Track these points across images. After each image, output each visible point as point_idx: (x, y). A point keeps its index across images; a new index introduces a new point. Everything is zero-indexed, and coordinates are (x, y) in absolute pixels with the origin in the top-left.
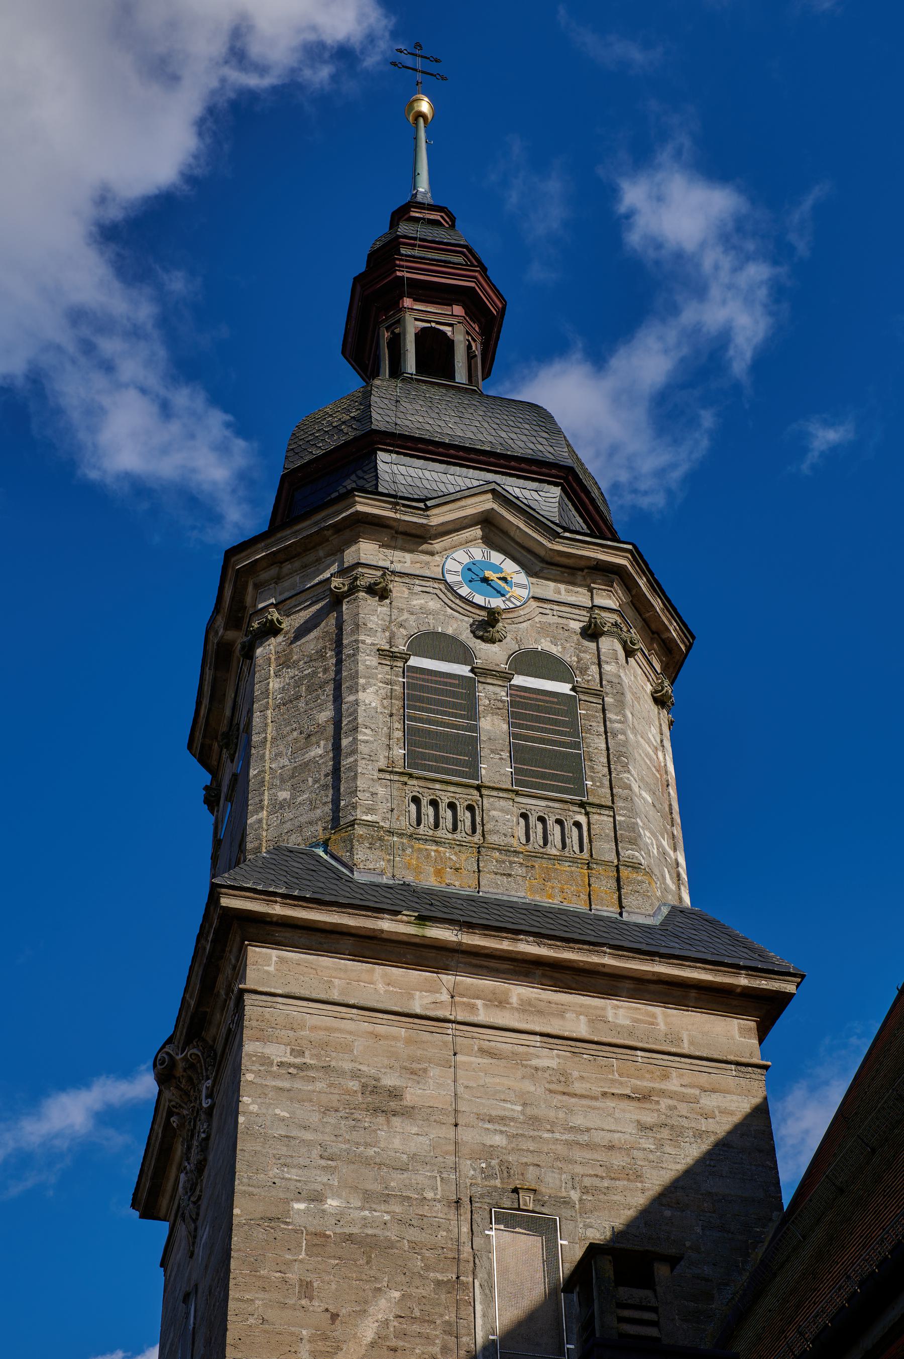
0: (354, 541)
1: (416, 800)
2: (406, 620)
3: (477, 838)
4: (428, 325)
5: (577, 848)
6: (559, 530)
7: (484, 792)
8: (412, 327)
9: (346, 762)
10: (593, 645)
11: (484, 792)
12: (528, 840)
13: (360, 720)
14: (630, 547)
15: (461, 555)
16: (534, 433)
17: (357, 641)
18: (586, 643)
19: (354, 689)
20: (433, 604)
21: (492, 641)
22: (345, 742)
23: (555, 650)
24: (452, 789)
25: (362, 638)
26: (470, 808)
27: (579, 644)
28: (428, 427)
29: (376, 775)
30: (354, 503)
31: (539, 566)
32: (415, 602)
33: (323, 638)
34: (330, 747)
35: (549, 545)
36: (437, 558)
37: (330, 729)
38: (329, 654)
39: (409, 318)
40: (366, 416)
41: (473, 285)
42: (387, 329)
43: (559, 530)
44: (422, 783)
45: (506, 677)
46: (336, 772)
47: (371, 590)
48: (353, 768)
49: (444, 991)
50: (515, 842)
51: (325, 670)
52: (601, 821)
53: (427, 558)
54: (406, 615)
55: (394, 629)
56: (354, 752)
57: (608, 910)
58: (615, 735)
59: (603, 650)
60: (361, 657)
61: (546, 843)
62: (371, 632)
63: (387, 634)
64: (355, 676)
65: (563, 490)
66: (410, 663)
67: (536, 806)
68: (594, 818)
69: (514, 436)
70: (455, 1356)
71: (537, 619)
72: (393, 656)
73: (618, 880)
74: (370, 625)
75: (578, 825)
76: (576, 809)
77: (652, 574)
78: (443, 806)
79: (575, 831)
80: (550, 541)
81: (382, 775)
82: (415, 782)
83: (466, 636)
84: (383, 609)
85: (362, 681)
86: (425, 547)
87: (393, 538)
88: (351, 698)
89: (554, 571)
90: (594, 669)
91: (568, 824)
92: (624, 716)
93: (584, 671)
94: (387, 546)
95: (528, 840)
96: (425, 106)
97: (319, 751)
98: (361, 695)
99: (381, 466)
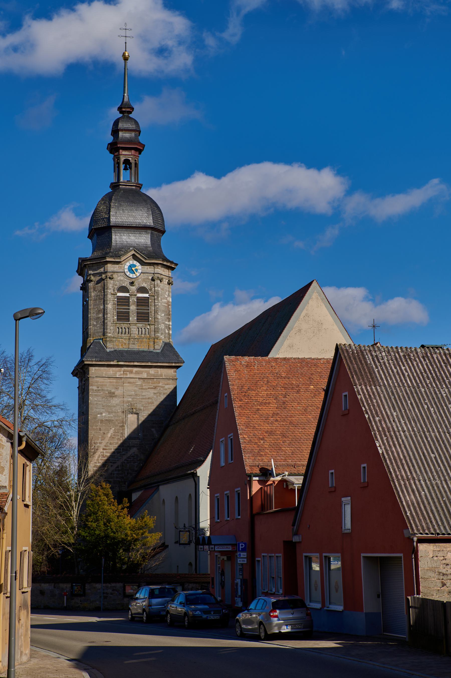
0: (107, 264)
1: (118, 328)
4: (126, 158)
6: (147, 258)
9: (106, 321)
10: (153, 282)
11: (131, 325)
15: (128, 264)
20: (122, 278)
22: (105, 316)
24: (125, 324)
25: (108, 291)
26: (128, 328)
27: (151, 282)
30: (106, 259)
31: (143, 264)
36: (123, 265)
37: (103, 310)
38: (102, 292)
39: (121, 156)
40: (109, 219)
42: (117, 158)
46: (104, 322)
47: (110, 278)
48: (107, 323)
50: (136, 335)
51: (102, 296)
52: (153, 327)
53: (121, 265)
54: (117, 282)
55: (114, 286)
56: (107, 319)
57: (151, 349)
58: (156, 306)
62: (110, 289)
64: (107, 301)
66: (117, 295)
72: (114, 294)
73: (154, 342)
74: (110, 287)
75: (148, 328)
76: (148, 325)
79: (147, 329)
82: (118, 324)
84: (112, 282)
85: (108, 302)
88: (106, 321)
89: (146, 264)
90: (153, 288)
93: (151, 290)
97: (101, 315)
99: (113, 237)
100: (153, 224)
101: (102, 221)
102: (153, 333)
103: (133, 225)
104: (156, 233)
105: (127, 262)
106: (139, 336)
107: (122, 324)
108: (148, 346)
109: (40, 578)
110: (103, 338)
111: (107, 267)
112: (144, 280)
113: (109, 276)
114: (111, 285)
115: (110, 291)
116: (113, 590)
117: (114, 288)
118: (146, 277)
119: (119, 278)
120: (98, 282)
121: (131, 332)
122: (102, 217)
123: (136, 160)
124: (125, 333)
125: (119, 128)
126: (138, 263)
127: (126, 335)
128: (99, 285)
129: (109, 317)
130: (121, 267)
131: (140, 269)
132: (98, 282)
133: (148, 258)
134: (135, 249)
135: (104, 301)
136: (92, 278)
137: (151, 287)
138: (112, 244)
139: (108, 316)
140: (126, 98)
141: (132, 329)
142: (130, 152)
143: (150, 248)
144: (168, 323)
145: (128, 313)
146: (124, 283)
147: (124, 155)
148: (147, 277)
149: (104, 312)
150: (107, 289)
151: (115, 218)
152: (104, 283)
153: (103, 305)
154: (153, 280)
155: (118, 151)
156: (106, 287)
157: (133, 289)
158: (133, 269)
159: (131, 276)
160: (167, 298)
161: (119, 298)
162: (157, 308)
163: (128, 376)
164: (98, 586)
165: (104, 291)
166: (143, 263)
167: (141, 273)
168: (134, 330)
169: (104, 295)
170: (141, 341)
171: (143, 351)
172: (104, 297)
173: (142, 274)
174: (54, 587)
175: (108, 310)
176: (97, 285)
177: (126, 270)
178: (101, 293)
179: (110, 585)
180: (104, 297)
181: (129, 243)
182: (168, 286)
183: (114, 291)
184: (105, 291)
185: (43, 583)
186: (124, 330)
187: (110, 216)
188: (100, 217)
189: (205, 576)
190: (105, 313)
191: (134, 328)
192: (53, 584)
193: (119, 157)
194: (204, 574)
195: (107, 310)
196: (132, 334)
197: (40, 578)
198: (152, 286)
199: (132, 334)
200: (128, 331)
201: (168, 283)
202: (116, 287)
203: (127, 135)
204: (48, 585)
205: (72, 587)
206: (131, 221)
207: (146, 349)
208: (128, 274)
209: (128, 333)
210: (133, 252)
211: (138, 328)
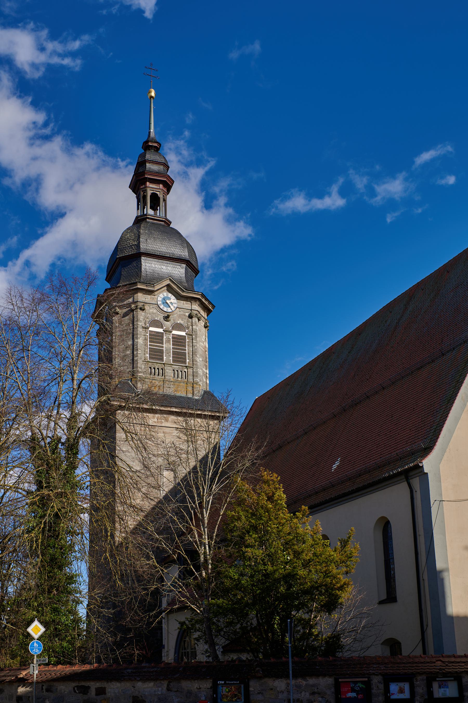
0: (137, 293)
1: (150, 368)
2: (148, 316)
3: (163, 377)
4: (153, 192)
5: (184, 378)
6: (185, 290)
7: (165, 365)
8: (149, 193)
9: (135, 358)
10: (191, 320)
11: (165, 365)
12: (174, 377)
13: (138, 348)
14: (201, 293)
15: (161, 296)
16: (180, 248)
17: (137, 324)
18: (189, 319)
19: (137, 338)
20: (155, 311)
21: (168, 321)
22: (135, 353)
23: (182, 322)
24: (158, 364)
25: (139, 323)
26: (162, 369)
27: (188, 320)
28: (154, 249)
29: (142, 362)
30: (137, 285)
31: (179, 297)
32: (151, 311)
33: (129, 319)
34: (131, 352)
35: (182, 294)
36: (156, 296)
37: (131, 347)
39: (148, 189)
40: (138, 246)
41: (165, 179)
43: (185, 290)
44: (152, 363)
45: (171, 332)
46: (133, 359)
48: (137, 361)
49: (156, 418)
50: (171, 378)
51: (130, 330)
52: (190, 370)
53: (153, 296)
54: (149, 315)
55: (146, 319)
56: (137, 356)
57: (190, 396)
59: (193, 322)
60: (139, 329)
61: (178, 377)
62: (141, 322)
63: (144, 321)
64: (137, 334)
65: (186, 265)
67: (176, 367)
68: (189, 370)
69: (175, 250)
70: (2, 305)
71: (178, 313)
72: (146, 328)
74: (141, 319)
75: (185, 372)
76: (185, 368)
77: (206, 297)
78: (156, 369)
79: (184, 373)
80: (182, 292)
81: (143, 362)
82: (150, 363)
83: (162, 320)
84: (143, 314)
85: (139, 336)
86: (153, 294)
87: (146, 292)
88: (136, 358)
89: (183, 299)
90: (191, 327)
91: (183, 372)
92: (197, 341)
94: (144, 294)
95: (174, 377)
96: (153, 94)
97: (129, 352)
98: (139, 340)
100: (188, 257)
101: (130, 249)
102: (190, 378)
103: (166, 256)
104: (190, 270)
105: (160, 293)
106: (174, 379)
107: (155, 364)
108: (186, 392)
109: (129, 671)
110: (132, 379)
111: (138, 296)
112: (180, 316)
113: (140, 306)
114: (142, 317)
115: (141, 324)
116: (313, 693)
117: (146, 321)
118: (182, 313)
119: (151, 311)
120: (125, 315)
121: (166, 374)
122: (129, 244)
123: (164, 196)
124: (159, 375)
125: (146, 159)
126: (172, 296)
127: (159, 377)
128: (127, 317)
129: (140, 354)
130: (154, 298)
131: (175, 303)
132: (125, 315)
133: (186, 290)
134: (171, 278)
135: (133, 336)
136: (118, 310)
137: (188, 325)
138: (142, 274)
139: (139, 352)
140: (152, 134)
141: (167, 371)
142: (158, 186)
143: (185, 283)
144: (205, 371)
145: (162, 352)
146: (157, 317)
147: (151, 188)
148: (184, 313)
149: (134, 348)
150: (137, 321)
151: (145, 245)
152: (133, 315)
153: (131, 340)
154: (191, 317)
155: (145, 184)
156: (135, 319)
157: (168, 325)
158: (168, 302)
159: (165, 309)
160: (204, 342)
161: (152, 334)
162: (196, 349)
163: (163, 425)
164: (280, 684)
165: (133, 324)
166: (179, 297)
167: (177, 307)
168: (169, 372)
169: (133, 328)
170: (178, 385)
171: (181, 397)
172: (133, 331)
173: (178, 309)
174: (169, 689)
175: (139, 346)
176: (122, 319)
177: (159, 303)
178: (130, 326)
179: (305, 683)
180: (133, 331)
181: (161, 275)
182: (204, 329)
183: (145, 324)
184: (135, 323)
185: (139, 681)
186: (157, 371)
187: (139, 243)
188: (127, 245)
189: (453, 659)
190: (135, 349)
191: (169, 370)
192: (165, 683)
193: (146, 190)
194: (449, 656)
195: (137, 345)
196: (168, 376)
197: (129, 671)
198: (189, 323)
199: (168, 376)
200: (161, 373)
201: (204, 325)
202: (148, 320)
203: (155, 168)
204: (151, 684)
205: (215, 688)
206: (164, 251)
207: (183, 395)
208: (162, 307)
209: (161, 375)
210: (168, 282)
211: (174, 370)
